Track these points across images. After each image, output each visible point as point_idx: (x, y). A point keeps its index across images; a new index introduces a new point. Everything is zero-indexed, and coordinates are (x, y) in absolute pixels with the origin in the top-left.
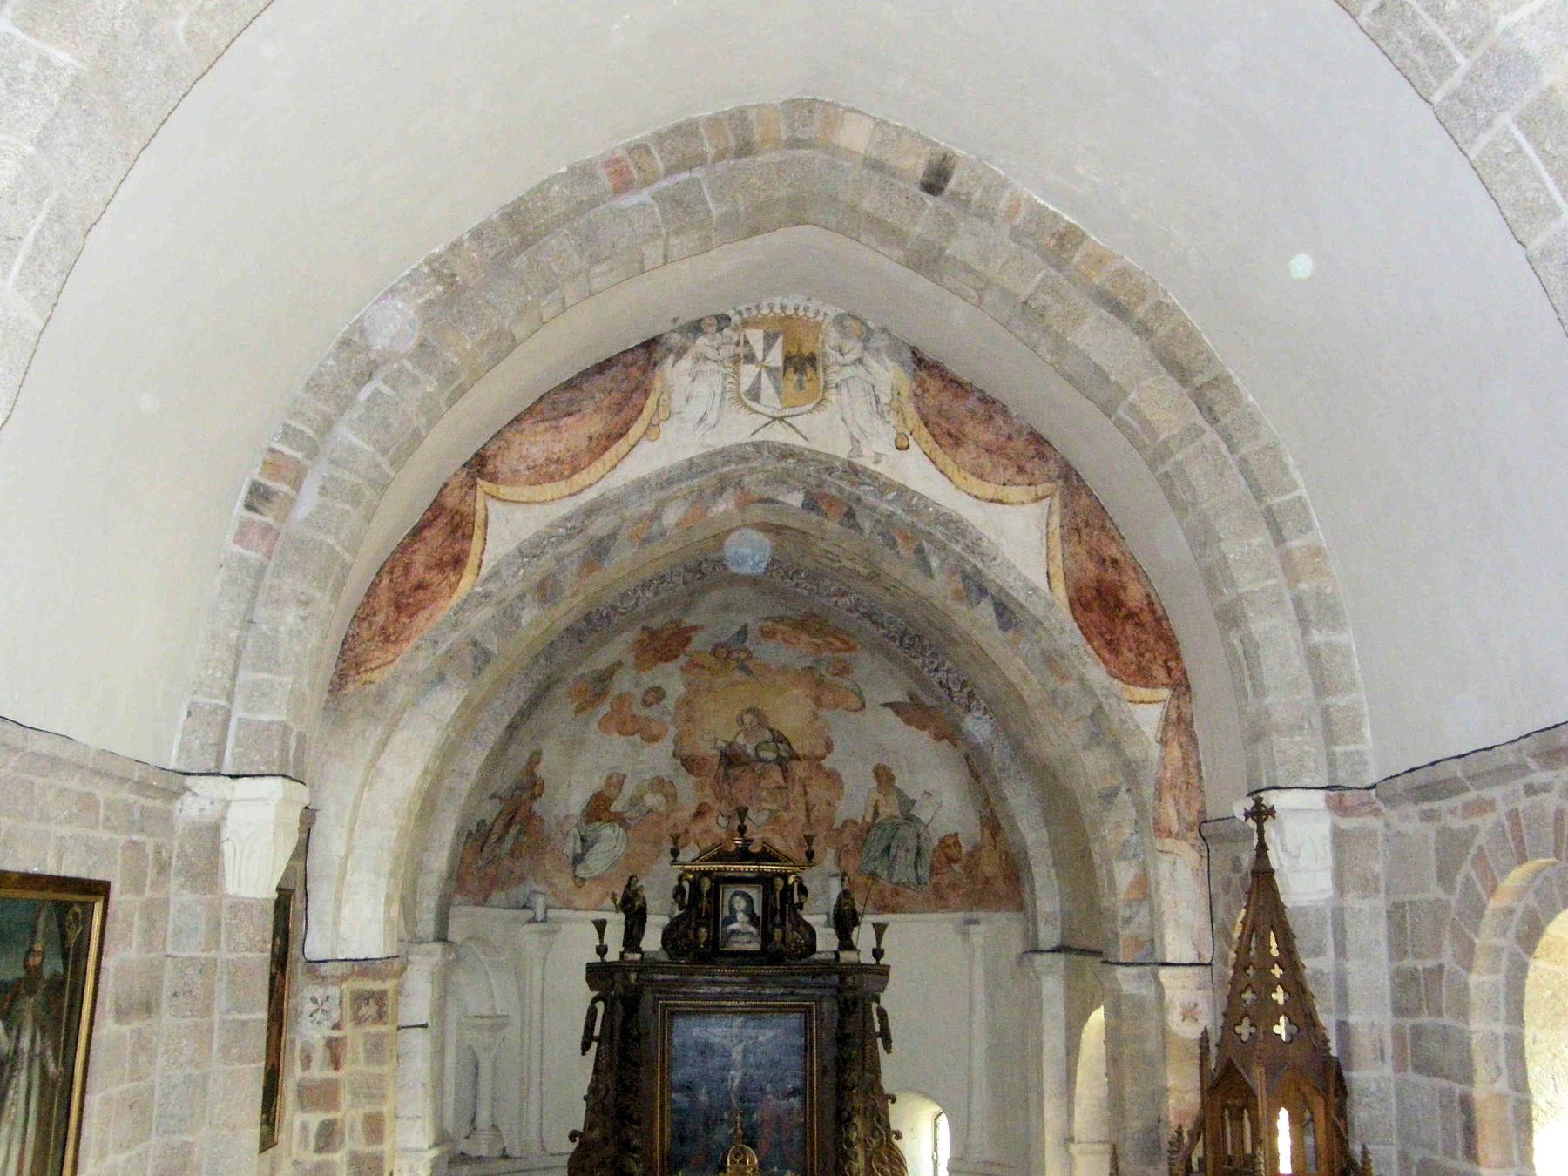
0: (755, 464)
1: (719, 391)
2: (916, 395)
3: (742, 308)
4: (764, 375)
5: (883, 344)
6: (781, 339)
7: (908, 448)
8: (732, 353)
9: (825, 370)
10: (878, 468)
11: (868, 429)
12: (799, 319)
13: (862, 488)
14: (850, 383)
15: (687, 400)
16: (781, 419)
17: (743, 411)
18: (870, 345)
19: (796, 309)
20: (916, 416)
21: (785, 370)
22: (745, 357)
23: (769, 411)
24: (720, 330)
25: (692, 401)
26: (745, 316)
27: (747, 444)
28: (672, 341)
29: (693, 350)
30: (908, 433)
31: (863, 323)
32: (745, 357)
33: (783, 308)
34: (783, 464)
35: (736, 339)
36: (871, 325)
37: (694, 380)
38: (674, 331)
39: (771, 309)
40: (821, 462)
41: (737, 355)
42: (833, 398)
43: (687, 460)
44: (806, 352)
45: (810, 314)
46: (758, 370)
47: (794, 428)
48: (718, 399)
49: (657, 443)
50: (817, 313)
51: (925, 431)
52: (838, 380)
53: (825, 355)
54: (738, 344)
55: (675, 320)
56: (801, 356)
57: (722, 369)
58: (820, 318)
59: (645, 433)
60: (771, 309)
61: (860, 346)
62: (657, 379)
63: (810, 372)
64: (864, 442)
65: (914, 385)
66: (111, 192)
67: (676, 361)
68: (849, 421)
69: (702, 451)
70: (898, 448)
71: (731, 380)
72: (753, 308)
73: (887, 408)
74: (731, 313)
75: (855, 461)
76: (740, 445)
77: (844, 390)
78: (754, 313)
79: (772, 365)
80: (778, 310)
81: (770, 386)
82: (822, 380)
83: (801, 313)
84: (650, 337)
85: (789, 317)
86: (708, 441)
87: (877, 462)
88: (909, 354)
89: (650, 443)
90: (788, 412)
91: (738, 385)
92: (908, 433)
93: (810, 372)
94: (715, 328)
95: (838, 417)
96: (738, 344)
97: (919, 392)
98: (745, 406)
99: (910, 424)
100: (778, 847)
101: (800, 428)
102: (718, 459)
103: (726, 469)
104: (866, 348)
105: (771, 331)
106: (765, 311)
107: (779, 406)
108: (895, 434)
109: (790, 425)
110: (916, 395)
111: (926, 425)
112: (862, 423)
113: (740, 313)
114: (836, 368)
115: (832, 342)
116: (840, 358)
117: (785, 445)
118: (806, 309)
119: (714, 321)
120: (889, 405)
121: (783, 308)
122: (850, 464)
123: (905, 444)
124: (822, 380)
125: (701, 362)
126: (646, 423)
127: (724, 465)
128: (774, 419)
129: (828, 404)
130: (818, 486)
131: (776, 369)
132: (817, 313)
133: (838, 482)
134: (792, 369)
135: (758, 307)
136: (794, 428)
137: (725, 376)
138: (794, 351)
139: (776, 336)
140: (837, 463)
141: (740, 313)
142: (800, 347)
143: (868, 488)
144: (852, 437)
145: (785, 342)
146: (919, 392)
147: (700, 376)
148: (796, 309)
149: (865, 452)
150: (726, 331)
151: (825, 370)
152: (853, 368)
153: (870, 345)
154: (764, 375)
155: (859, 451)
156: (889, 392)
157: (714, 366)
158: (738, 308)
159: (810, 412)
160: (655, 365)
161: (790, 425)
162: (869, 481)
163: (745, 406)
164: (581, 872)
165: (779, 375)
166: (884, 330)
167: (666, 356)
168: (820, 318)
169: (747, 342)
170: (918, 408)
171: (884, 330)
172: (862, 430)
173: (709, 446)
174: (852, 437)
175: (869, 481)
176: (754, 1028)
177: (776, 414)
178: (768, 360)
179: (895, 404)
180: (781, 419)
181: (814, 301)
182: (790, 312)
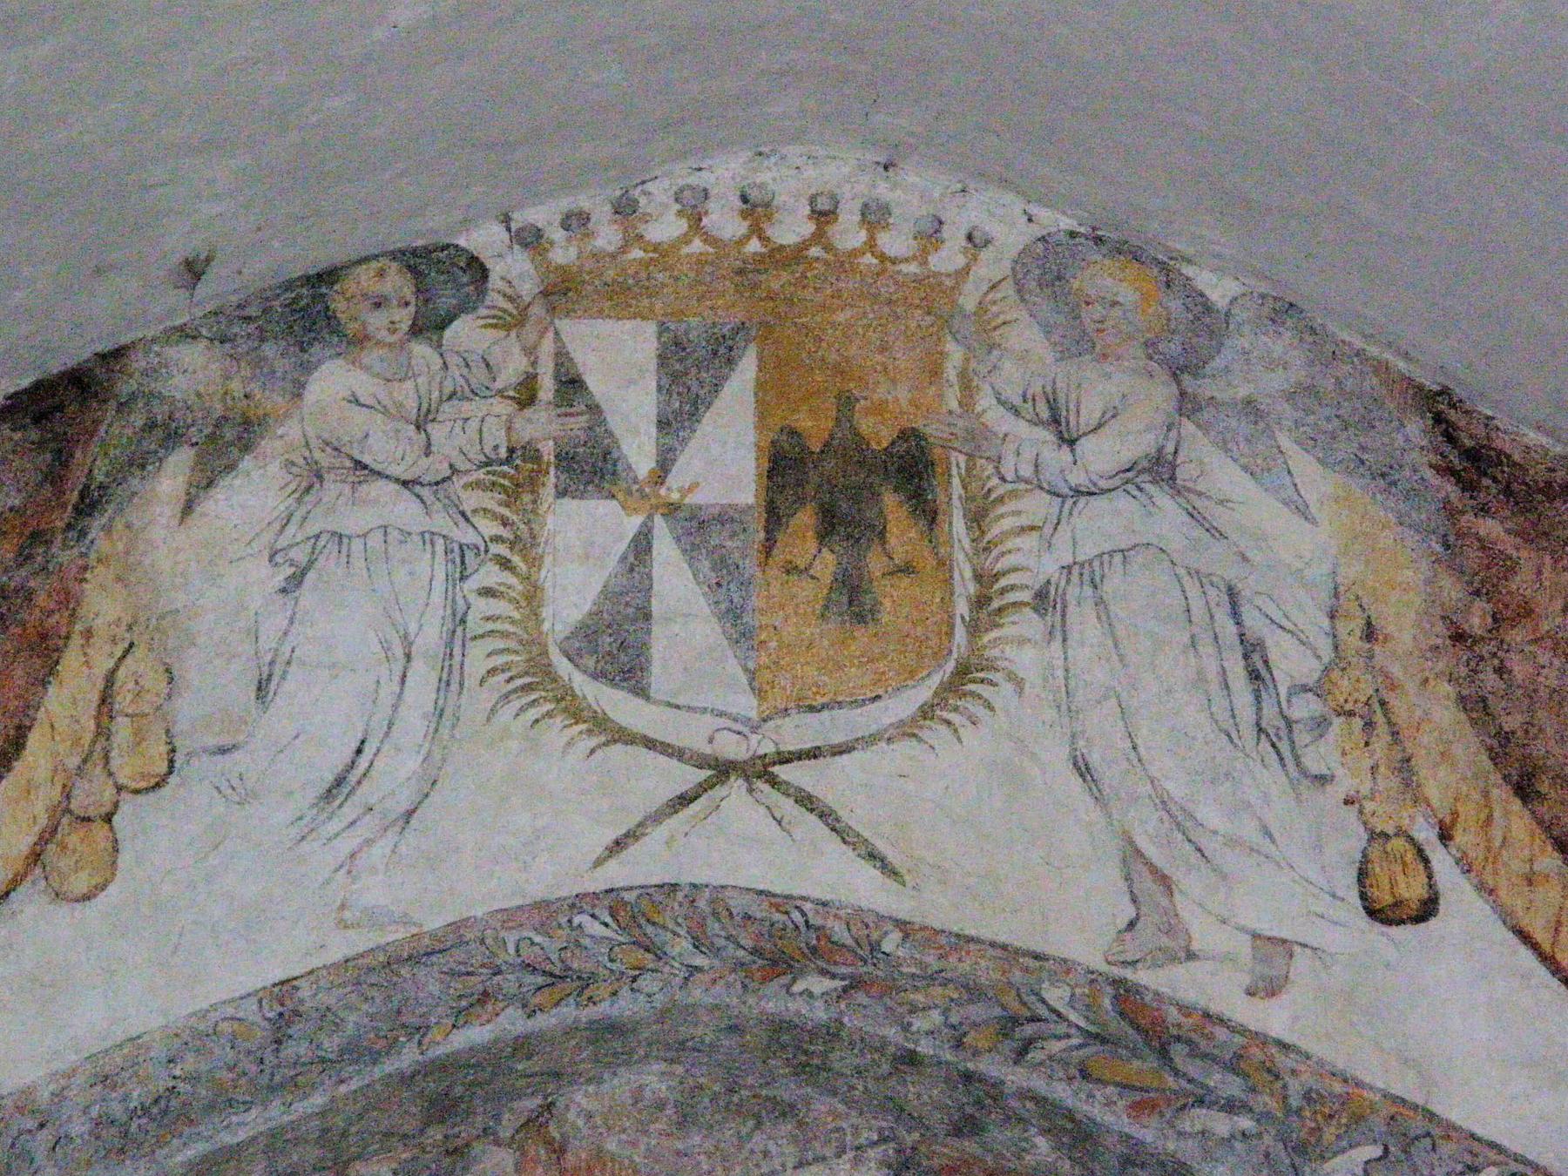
0: (626, 1006)
1: (431, 635)
2: (1459, 637)
3: (542, 215)
4: (665, 547)
5: (1277, 381)
6: (747, 370)
7: (1427, 909)
8: (496, 437)
9: (977, 519)
10: (1273, 1019)
11: (1210, 815)
12: (844, 263)
13: (1198, 1119)
14: (1113, 585)
15: (261, 688)
16: (760, 771)
17: (557, 732)
18: (1205, 388)
19: (823, 216)
20: (1469, 748)
21: (774, 517)
22: (566, 460)
23: (693, 734)
24: (429, 326)
25: (291, 689)
26: (563, 254)
27: (579, 903)
28: (178, 386)
29: (291, 430)
30: (1425, 834)
31: (1169, 276)
32: (566, 460)
33: (755, 209)
34: (773, 1001)
35: (512, 369)
36: (1219, 289)
37: (296, 580)
38: (186, 334)
39: (696, 219)
40: (973, 992)
41: (521, 453)
42: (1025, 660)
43: (259, 996)
44: (879, 433)
45: (895, 242)
46: (633, 523)
47: (826, 815)
48: (423, 677)
49: (92, 910)
50: (931, 235)
51: (1516, 821)
52: (1049, 567)
53: (977, 439)
54: (526, 395)
55: (194, 270)
56: (853, 450)
57: (441, 522)
58: (947, 258)
59: (35, 856)
60: (696, 219)
61: (1161, 394)
62: (99, 575)
63: (902, 532)
64: (1191, 884)
65: (1452, 590)
66: (658, 834)
67: (205, 480)
68: (1109, 775)
69: (339, 948)
70: (1373, 913)
71: (490, 575)
72: (601, 214)
73: (1305, 708)
74: (485, 239)
75: (1142, 977)
76: (544, 912)
77: (1084, 622)
78: (607, 236)
79: (709, 496)
80: (726, 222)
81: (701, 604)
82: (963, 571)
83: (848, 234)
84: (55, 366)
85: (779, 257)
86: (374, 892)
87: (1268, 988)
88: (1416, 428)
89: (63, 914)
90: (796, 732)
91: (533, 597)
92: (1425, 834)
93: (902, 532)
94: (404, 317)
95: (1057, 756)
96: (526, 395)
97: (1477, 620)
98: (574, 709)
99: (1437, 786)
100: (676, 234)
101: (856, 818)
102: (430, 983)
103: (476, 1034)
104: (1187, 405)
105: (694, 326)
106: (666, 227)
107: (747, 705)
108: (1355, 840)
109: (806, 801)
110: (1459, 637)
111: (1524, 790)
112: (1175, 788)
113: (531, 240)
114: (1037, 507)
115: (1011, 378)
116: (1056, 457)
117: (781, 902)
118: (875, 216)
119: (397, 283)
120: (1318, 690)
121: (755, 209)
122: (1126, 996)
123: (1412, 890)
124: (963, 571)
125: (332, 488)
126: (40, 808)
127: (462, 1016)
128: (723, 770)
129: (1002, 694)
130: (966, 1126)
131: (726, 518)
132: (931, 235)
133: (1061, 1092)
134: (805, 518)
135: (625, 209)
136: (826, 815)
137: (461, 560)
138: (814, 426)
139: (723, 353)
140: (1056, 995)
141: (531, 240)
142: (846, 402)
143: (1221, 1124)
144: (1132, 854)
145: (769, 392)
146: (1477, 620)
147: (330, 564)
148: (823, 216)
149: (1204, 933)
150: (465, 332)
151: (977, 519)
152: (1122, 502)
153: (1205, 388)
154: (665, 547)
155: (1172, 925)
156: (1314, 622)
157: (405, 510)
158: (525, 216)
159: (907, 730)
160: (88, 505)
161: (806, 801)
162: (1233, 1087)
163: (574, 709)
164: (634, 985)
165: (744, 547)
166: (1283, 311)
167: (139, 462)
168: (947, 258)
169: (571, 384)
170: (1475, 706)
171: (1283, 311)
172: (1179, 819)
173: (373, 918)
174: (1132, 854)
175: (1233, 1087)
176: (689, 1011)
177: (732, 748)
178: (676, 480)
179: (1355, 686)
180: (760, 771)
181: (911, 176)
182: (791, 229)
